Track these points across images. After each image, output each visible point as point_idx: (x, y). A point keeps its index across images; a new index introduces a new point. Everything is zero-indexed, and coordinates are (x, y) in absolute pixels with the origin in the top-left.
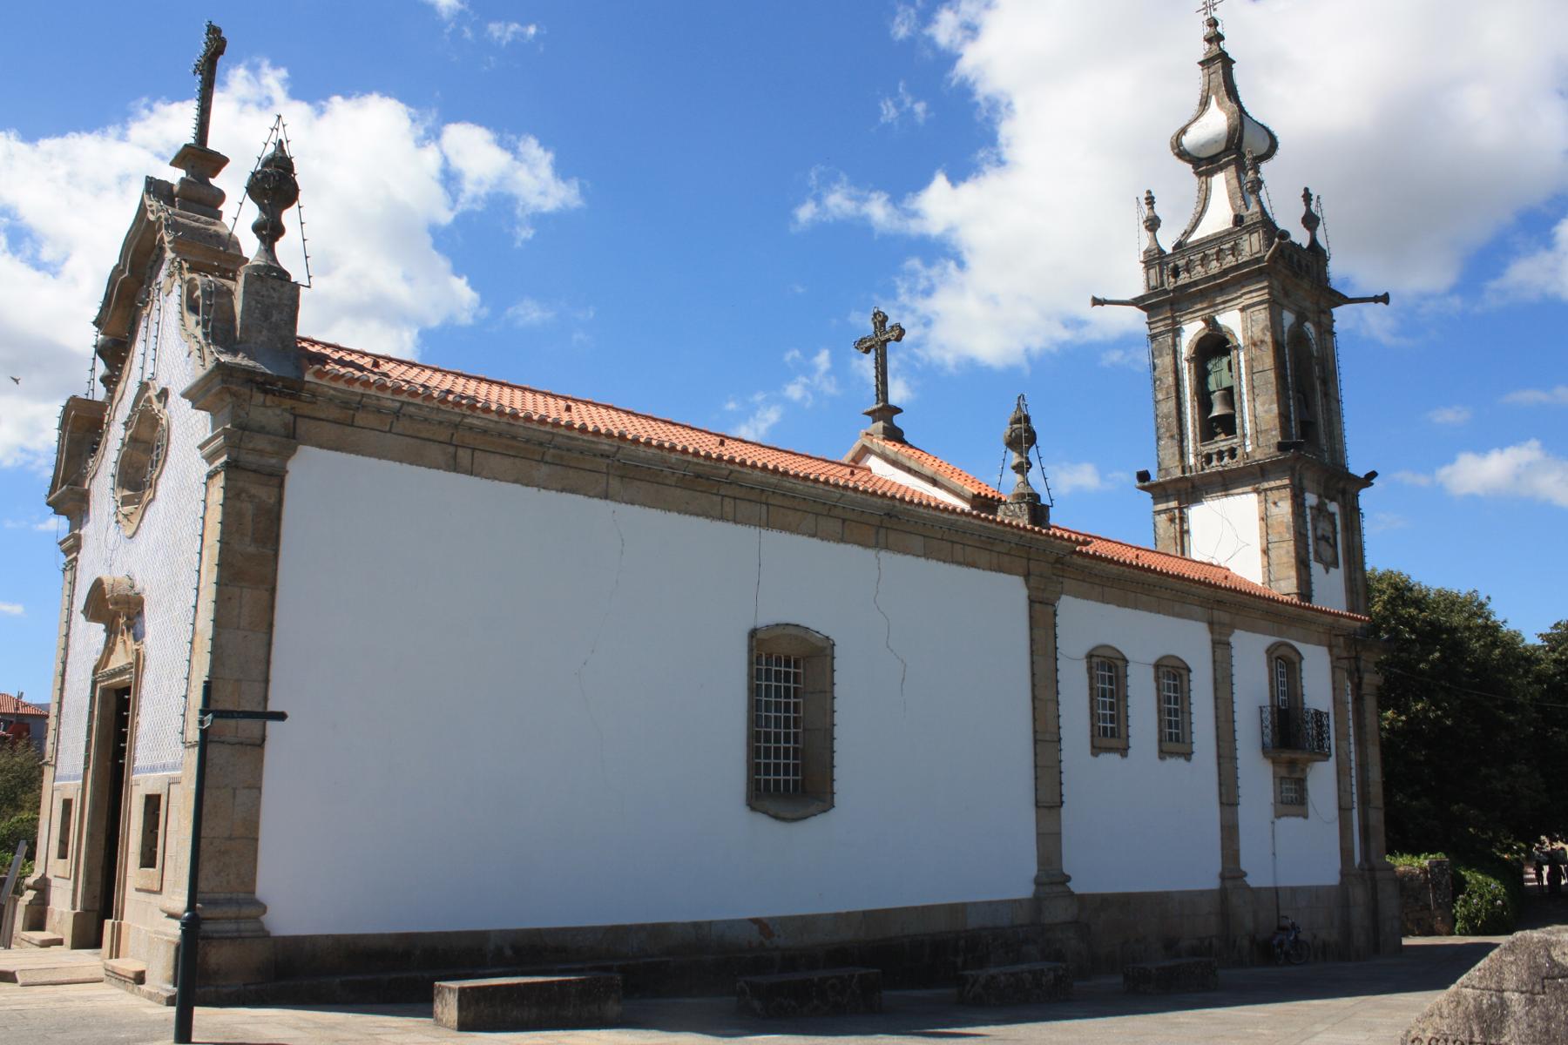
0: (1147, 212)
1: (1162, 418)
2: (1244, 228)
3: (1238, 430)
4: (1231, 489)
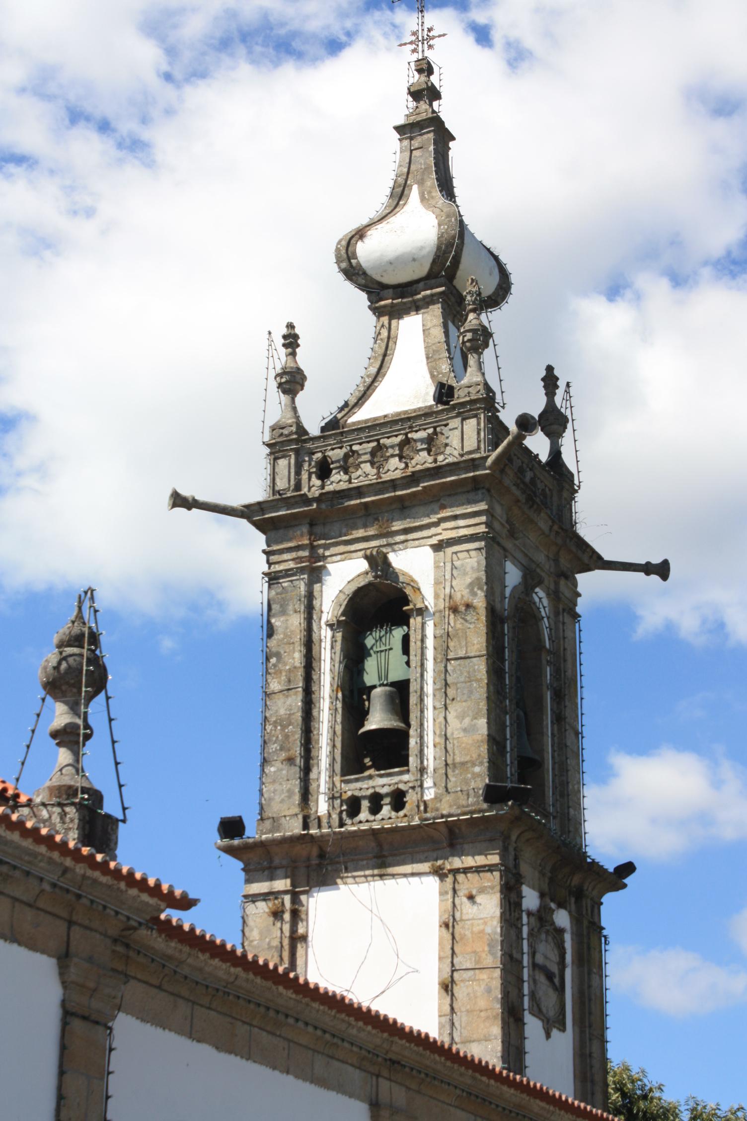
0: (284, 359)
1: (275, 724)
2: (454, 407)
3: (412, 760)
4: (390, 865)
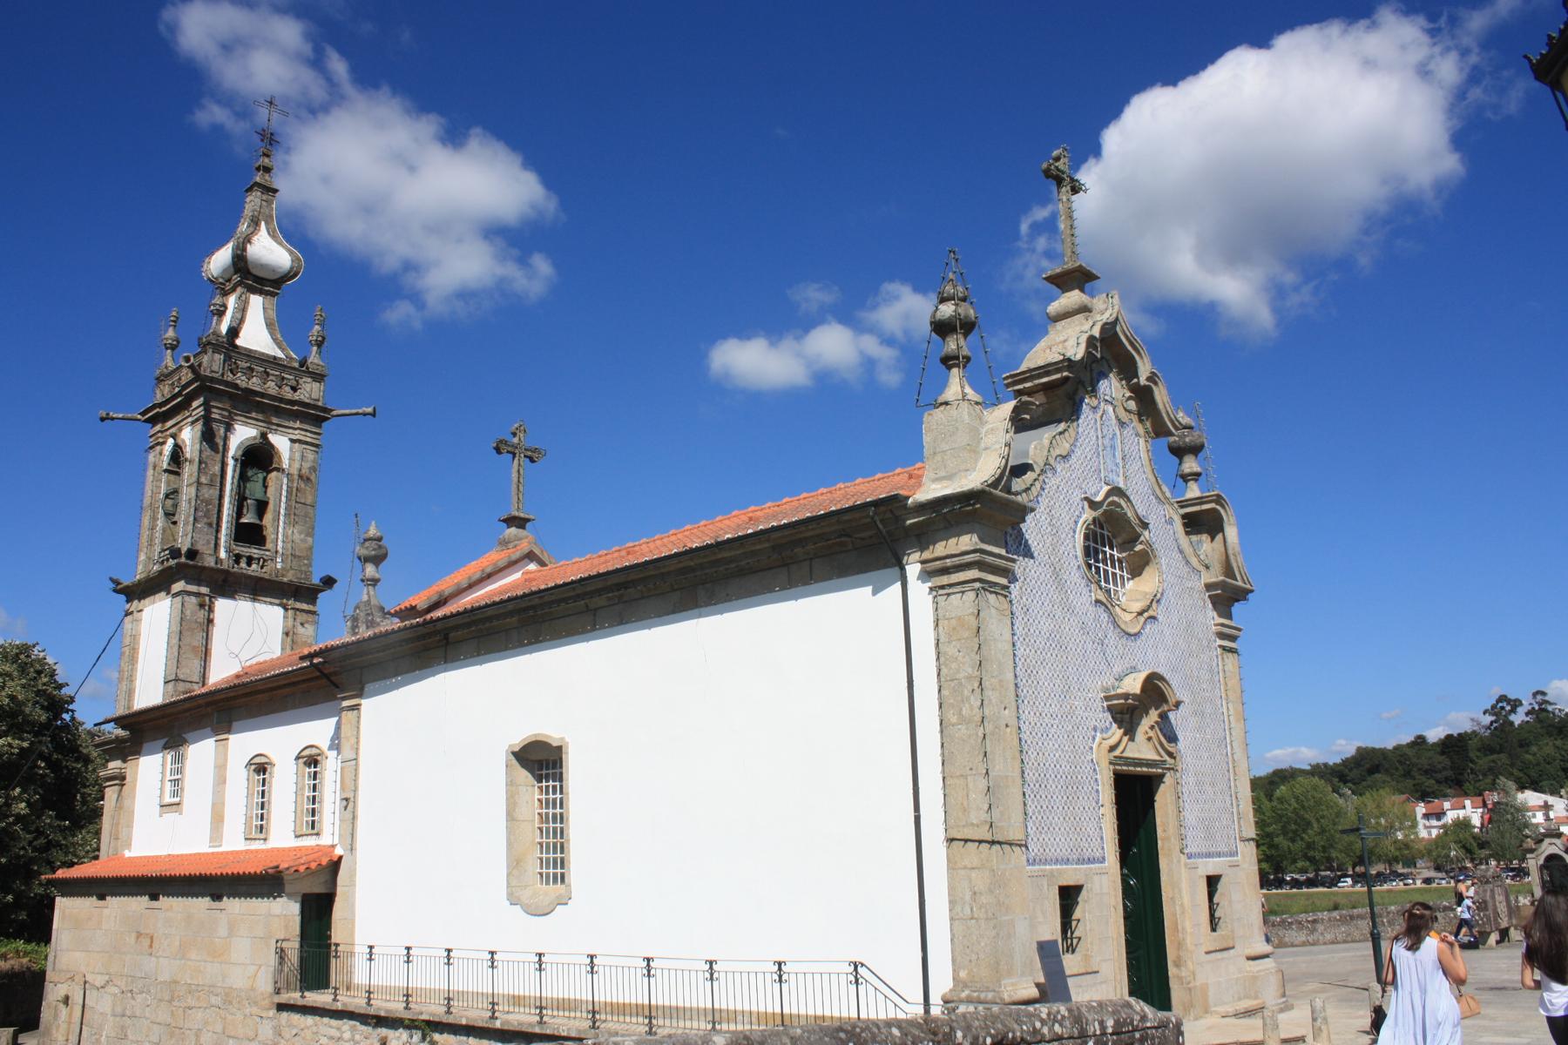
1: (202, 501)
4: (259, 596)
